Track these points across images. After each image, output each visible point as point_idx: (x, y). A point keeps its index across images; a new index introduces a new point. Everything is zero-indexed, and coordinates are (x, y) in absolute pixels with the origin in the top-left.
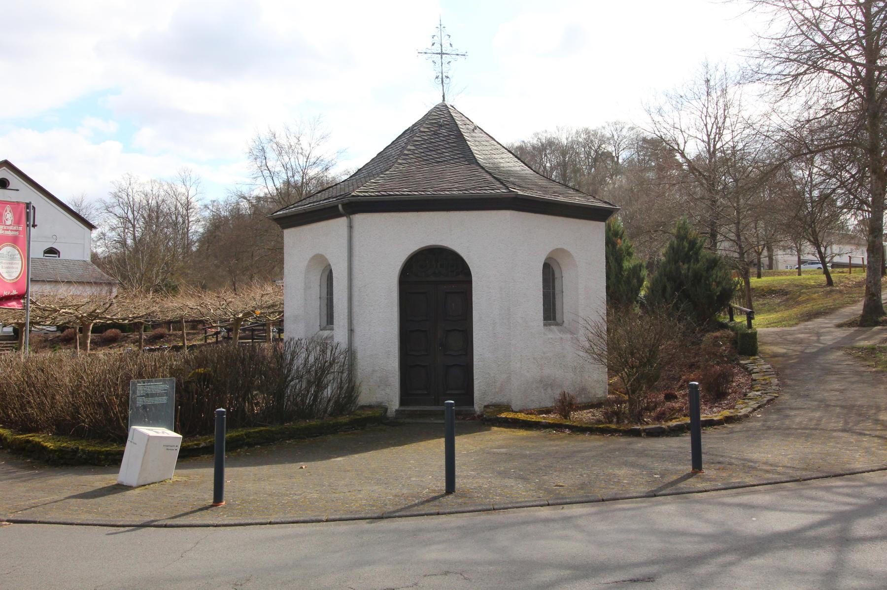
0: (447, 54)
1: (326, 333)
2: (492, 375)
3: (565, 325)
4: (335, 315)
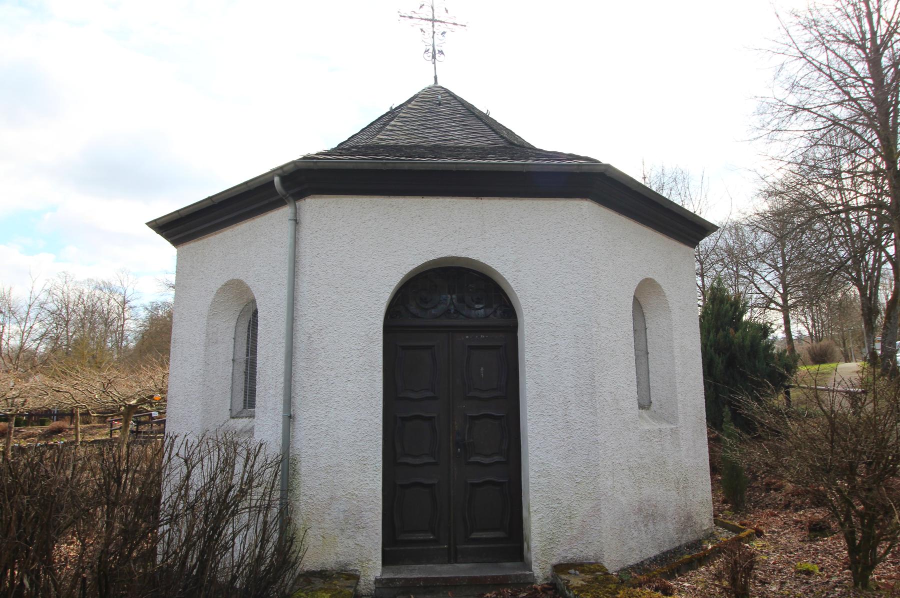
0: (441, 22)
1: (241, 424)
2: (565, 503)
3: (653, 407)
4: (259, 388)
